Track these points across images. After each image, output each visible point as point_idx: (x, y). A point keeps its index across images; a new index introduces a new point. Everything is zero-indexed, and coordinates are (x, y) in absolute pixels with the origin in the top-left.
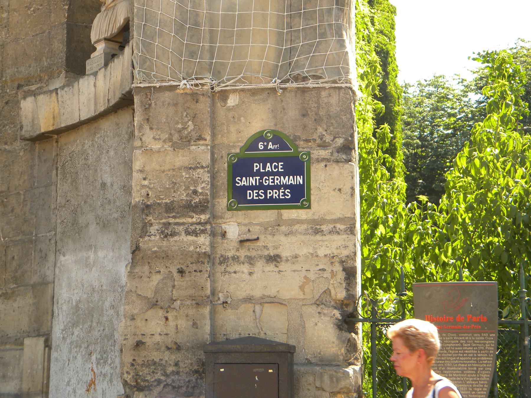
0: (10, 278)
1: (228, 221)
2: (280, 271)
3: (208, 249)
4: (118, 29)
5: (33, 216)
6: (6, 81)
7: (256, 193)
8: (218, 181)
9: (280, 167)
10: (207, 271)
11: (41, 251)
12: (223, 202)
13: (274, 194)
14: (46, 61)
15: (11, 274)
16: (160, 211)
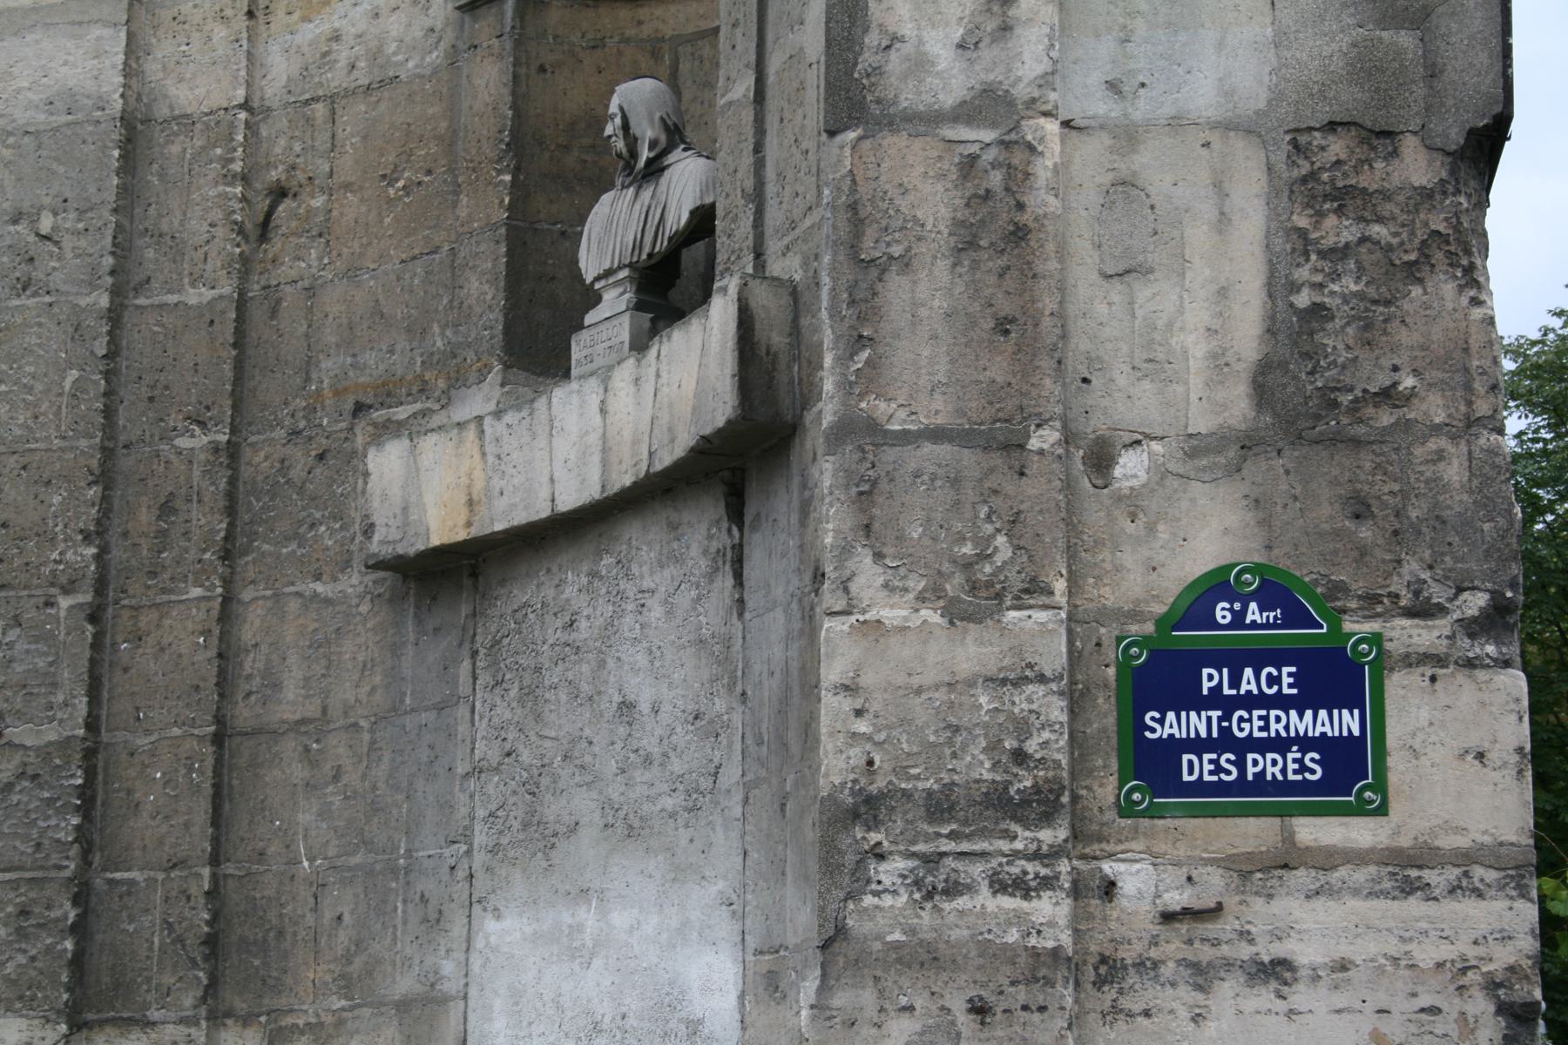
0: (328, 978)
1: (1120, 847)
2: (1291, 1013)
3: (1066, 939)
4: (670, 239)
5: (400, 797)
6: (319, 391)
7: (1211, 761)
8: (1089, 722)
9: (1286, 680)
10: (1062, 1008)
11: (424, 899)
12: (1105, 789)
13: (1269, 765)
14: (443, 334)
15: (332, 967)
16: (910, 816)
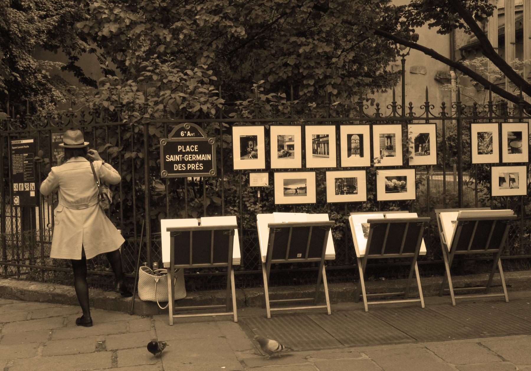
9: (196, 148)
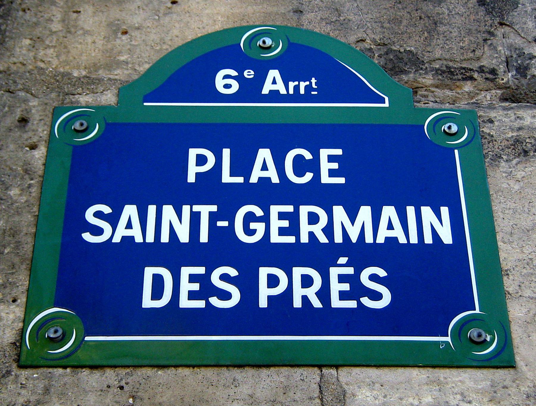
7: (193, 278)
9: (325, 166)
13: (302, 287)
